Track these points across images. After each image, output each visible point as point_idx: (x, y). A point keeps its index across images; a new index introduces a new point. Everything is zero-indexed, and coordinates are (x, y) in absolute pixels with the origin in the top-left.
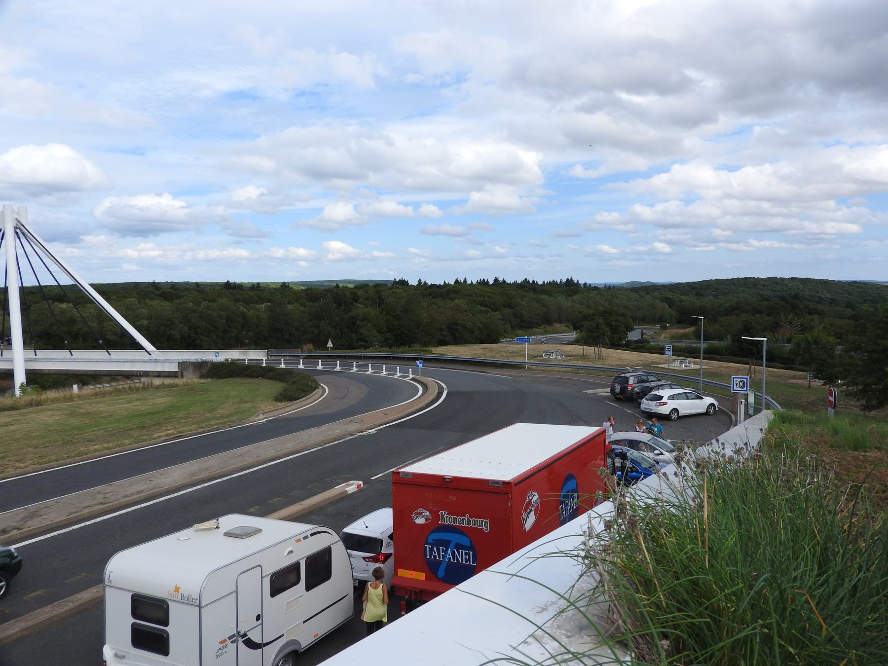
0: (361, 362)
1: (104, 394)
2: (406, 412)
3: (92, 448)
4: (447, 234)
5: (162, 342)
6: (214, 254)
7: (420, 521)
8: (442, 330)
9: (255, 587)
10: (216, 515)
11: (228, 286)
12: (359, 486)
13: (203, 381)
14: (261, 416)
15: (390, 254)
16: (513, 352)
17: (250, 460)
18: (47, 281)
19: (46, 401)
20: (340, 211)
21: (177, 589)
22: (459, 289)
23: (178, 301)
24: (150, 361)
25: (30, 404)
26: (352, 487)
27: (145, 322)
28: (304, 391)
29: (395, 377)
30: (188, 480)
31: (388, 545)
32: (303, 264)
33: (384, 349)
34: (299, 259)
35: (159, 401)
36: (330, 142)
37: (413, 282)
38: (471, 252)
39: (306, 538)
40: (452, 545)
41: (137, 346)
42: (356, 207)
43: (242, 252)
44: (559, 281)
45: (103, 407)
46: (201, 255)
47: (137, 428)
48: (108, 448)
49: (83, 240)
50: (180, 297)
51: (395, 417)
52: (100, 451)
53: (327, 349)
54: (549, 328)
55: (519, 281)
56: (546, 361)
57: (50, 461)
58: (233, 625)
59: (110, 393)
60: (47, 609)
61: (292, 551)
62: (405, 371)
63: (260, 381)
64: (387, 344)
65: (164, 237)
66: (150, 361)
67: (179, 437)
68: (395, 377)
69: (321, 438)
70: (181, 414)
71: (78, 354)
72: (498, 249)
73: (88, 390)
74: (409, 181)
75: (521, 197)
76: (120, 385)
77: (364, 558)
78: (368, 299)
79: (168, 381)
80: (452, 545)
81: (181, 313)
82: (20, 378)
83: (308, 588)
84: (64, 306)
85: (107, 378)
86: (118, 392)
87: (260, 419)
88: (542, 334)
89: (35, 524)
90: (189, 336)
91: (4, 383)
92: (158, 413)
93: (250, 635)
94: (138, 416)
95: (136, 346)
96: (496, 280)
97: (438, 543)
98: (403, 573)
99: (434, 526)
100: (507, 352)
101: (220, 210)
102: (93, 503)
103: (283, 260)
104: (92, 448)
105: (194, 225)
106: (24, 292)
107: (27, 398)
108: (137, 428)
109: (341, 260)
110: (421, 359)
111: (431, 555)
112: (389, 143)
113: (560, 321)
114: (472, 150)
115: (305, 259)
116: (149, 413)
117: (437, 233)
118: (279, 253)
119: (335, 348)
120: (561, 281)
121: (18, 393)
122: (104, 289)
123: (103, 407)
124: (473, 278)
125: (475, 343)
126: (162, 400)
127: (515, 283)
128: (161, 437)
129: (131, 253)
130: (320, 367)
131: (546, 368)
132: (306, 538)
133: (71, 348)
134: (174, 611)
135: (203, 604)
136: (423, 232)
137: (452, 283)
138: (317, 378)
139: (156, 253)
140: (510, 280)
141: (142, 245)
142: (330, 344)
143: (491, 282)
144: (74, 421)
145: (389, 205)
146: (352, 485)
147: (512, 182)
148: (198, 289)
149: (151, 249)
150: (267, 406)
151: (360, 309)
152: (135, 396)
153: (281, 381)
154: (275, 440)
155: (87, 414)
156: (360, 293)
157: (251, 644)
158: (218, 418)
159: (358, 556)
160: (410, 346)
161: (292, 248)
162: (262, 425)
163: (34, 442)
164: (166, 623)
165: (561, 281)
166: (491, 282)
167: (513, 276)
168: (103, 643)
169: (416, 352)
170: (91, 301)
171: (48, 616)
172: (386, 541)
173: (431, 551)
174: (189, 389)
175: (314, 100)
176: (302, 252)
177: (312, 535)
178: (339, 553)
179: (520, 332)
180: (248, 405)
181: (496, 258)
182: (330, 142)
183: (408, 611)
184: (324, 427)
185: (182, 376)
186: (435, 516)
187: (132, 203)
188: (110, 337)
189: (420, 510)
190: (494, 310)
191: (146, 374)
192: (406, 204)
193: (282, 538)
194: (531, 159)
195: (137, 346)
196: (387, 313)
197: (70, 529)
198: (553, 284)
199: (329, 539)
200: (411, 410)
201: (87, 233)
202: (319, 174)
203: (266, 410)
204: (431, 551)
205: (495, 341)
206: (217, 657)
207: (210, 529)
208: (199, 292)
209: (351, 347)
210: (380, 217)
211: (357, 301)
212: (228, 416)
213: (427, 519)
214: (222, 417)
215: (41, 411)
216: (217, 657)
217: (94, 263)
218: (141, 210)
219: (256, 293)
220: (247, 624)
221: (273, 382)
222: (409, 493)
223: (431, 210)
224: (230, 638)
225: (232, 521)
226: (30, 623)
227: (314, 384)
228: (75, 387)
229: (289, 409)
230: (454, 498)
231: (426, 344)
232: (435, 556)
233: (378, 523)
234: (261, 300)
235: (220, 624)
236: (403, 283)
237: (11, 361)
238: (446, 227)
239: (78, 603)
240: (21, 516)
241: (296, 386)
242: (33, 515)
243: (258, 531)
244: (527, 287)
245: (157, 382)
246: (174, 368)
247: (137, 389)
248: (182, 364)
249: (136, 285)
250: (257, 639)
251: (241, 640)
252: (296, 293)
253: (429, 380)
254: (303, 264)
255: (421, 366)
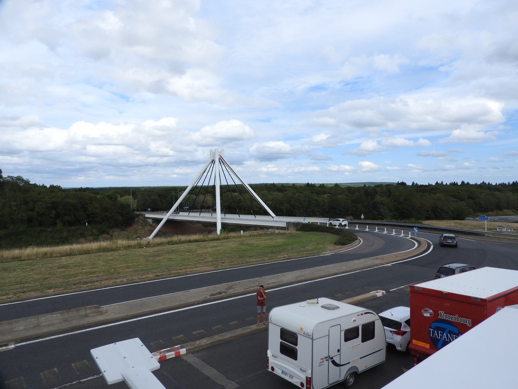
0: (380, 227)
1: (254, 236)
2: (409, 256)
3: (252, 260)
4: (434, 156)
5: (279, 212)
6: (303, 169)
7: (427, 315)
8: (428, 211)
9: (337, 336)
10: (317, 297)
11: (309, 186)
12: (383, 293)
13: (298, 232)
14: (328, 252)
15: (396, 168)
16: (476, 226)
17: (324, 273)
18: (231, 183)
19: (231, 237)
20: (370, 145)
21: (302, 329)
22: (439, 187)
23: (285, 192)
24: (273, 221)
25: (224, 238)
26: (380, 293)
27: (270, 203)
28: (350, 240)
29: (400, 236)
30: (295, 280)
31: (405, 327)
32: (347, 174)
33: (393, 220)
34: (345, 171)
35: (279, 240)
36: (364, 107)
37: (409, 183)
38: (448, 166)
39: (362, 314)
40: (447, 331)
41: (267, 214)
42: (379, 143)
43: (316, 168)
44: (507, 183)
45: (254, 241)
46: (296, 170)
47: (270, 253)
48: (259, 261)
49: (244, 164)
50: (286, 191)
51: (402, 258)
52: (255, 262)
53: (361, 219)
54: (499, 212)
55: (479, 183)
56: (499, 232)
57: (235, 264)
58: (327, 352)
59: (257, 236)
60: (240, 330)
61: (355, 320)
62: (406, 234)
63: (326, 234)
64: (395, 218)
65: (279, 161)
66: (273, 221)
67: (289, 259)
68: (400, 236)
69: (361, 266)
70: (289, 248)
71: (242, 217)
72: (467, 164)
73: (247, 233)
74: (414, 125)
75: (486, 132)
76: (261, 232)
77: (391, 331)
78: (382, 193)
79: (282, 231)
80: (447, 331)
81: (288, 198)
82: (219, 227)
83: (363, 341)
84: (235, 194)
85: (253, 228)
86: (260, 235)
87: (328, 253)
88: (495, 216)
89: (231, 291)
90: (290, 210)
91: (212, 228)
92: (279, 246)
93: (335, 359)
94: (270, 247)
95: (266, 214)
96: (463, 182)
97: (437, 329)
98: (414, 342)
99: (435, 318)
100: (472, 225)
101: (306, 147)
102: (254, 285)
103: (338, 172)
104: (252, 260)
105: (293, 155)
106: (221, 187)
107: (223, 235)
108: (270, 253)
109: (367, 171)
110: (416, 227)
111: (433, 335)
112: (405, 104)
113: (508, 208)
114: (457, 105)
115: (349, 171)
116: (274, 246)
117: (428, 155)
118: (335, 168)
119: (364, 219)
120: (509, 183)
121: (218, 232)
122: (255, 187)
123: (254, 241)
124: (447, 181)
125: (449, 219)
126: (280, 240)
127: (476, 185)
128: (281, 258)
129: (264, 169)
130: (357, 229)
131: (499, 237)
132: (362, 314)
133: (239, 213)
134: (300, 339)
135: (314, 338)
136: (419, 155)
137: (434, 184)
138: (356, 234)
139: (276, 169)
140: (472, 182)
141: (269, 166)
142: (362, 217)
143: (459, 184)
144: (243, 247)
145: (399, 140)
146: (380, 292)
147: (481, 123)
148: (294, 187)
149: (273, 167)
150: (331, 247)
151: (378, 198)
152: (267, 237)
153: (337, 234)
154: (336, 265)
155: (248, 244)
156: (378, 189)
157: (334, 363)
158: (307, 251)
159: (387, 330)
160: (408, 220)
161: (342, 166)
162: (329, 256)
163: (227, 255)
164: (296, 345)
165: (509, 183)
166: (459, 184)
167: (474, 180)
168: (267, 349)
169: (412, 223)
170: (247, 192)
171: (240, 333)
172: (403, 324)
173: (433, 333)
174: (292, 236)
175: (354, 87)
176: (347, 167)
177: (365, 313)
178: (378, 325)
179: (479, 214)
180: (321, 245)
181: (465, 169)
182: (364, 107)
183: (418, 363)
184: (362, 260)
185: (288, 229)
186: (436, 313)
187: (267, 145)
188: (255, 209)
189: (427, 309)
190: (462, 200)
191: (272, 227)
192: (409, 139)
193: (349, 313)
194: (495, 107)
195: (267, 214)
196: (395, 201)
197: (44, 339)
198: (503, 185)
199: (371, 317)
200: (412, 255)
201: (245, 160)
202: (360, 125)
203: (331, 248)
204: (433, 333)
205: (463, 219)
206: (320, 366)
207: (314, 303)
208: (294, 188)
209: (374, 219)
210: (394, 147)
211: (376, 193)
212: (312, 250)
213: (431, 314)
214: (308, 251)
215: (229, 241)
216: (320, 366)
217: (253, 174)
218: (270, 148)
219: (322, 189)
220: (333, 353)
221: (333, 235)
222: (419, 299)
223: (426, 142)
224: (326, 358)
225: (324, 301)
226: (233, 335)
227: (355, 237)
228: (242, 231)
229: (342, 249)
230: (448, 304)
231: (418, 219)
232: (436, 336)
233: (400, 313)
234: (325, 193)
235: (321, 351)
236: (403, 184)
237: (216, 218)
238: (434, 152)
239: (252, 330)
240: (225, 288)
241: (345, 237)
242: (230, 288)
243: (338, 307)
244: (484, 186)
245: (277, 231)
246: (284, 225)
247: (268, 234)
248: (288, 223)
249: (266, 185)
250: (338, 362)
251: (330, 360)
252: (342, 189)
253: (422, 239)
254: (347, 174)
255: (416, 231)
